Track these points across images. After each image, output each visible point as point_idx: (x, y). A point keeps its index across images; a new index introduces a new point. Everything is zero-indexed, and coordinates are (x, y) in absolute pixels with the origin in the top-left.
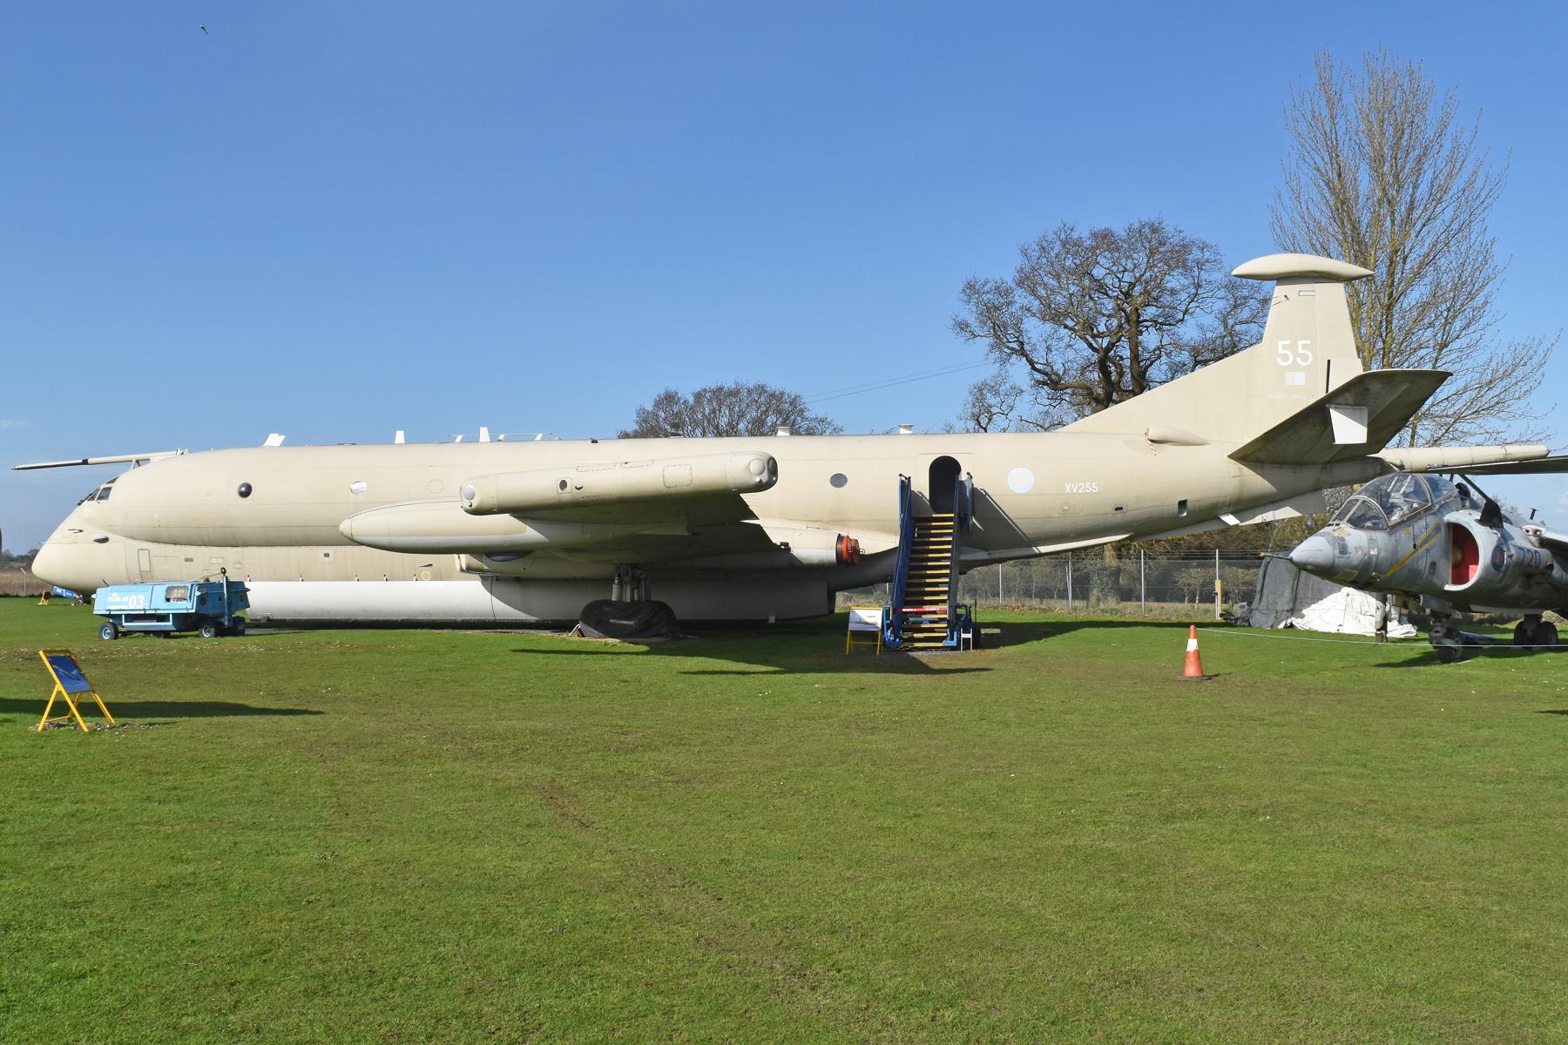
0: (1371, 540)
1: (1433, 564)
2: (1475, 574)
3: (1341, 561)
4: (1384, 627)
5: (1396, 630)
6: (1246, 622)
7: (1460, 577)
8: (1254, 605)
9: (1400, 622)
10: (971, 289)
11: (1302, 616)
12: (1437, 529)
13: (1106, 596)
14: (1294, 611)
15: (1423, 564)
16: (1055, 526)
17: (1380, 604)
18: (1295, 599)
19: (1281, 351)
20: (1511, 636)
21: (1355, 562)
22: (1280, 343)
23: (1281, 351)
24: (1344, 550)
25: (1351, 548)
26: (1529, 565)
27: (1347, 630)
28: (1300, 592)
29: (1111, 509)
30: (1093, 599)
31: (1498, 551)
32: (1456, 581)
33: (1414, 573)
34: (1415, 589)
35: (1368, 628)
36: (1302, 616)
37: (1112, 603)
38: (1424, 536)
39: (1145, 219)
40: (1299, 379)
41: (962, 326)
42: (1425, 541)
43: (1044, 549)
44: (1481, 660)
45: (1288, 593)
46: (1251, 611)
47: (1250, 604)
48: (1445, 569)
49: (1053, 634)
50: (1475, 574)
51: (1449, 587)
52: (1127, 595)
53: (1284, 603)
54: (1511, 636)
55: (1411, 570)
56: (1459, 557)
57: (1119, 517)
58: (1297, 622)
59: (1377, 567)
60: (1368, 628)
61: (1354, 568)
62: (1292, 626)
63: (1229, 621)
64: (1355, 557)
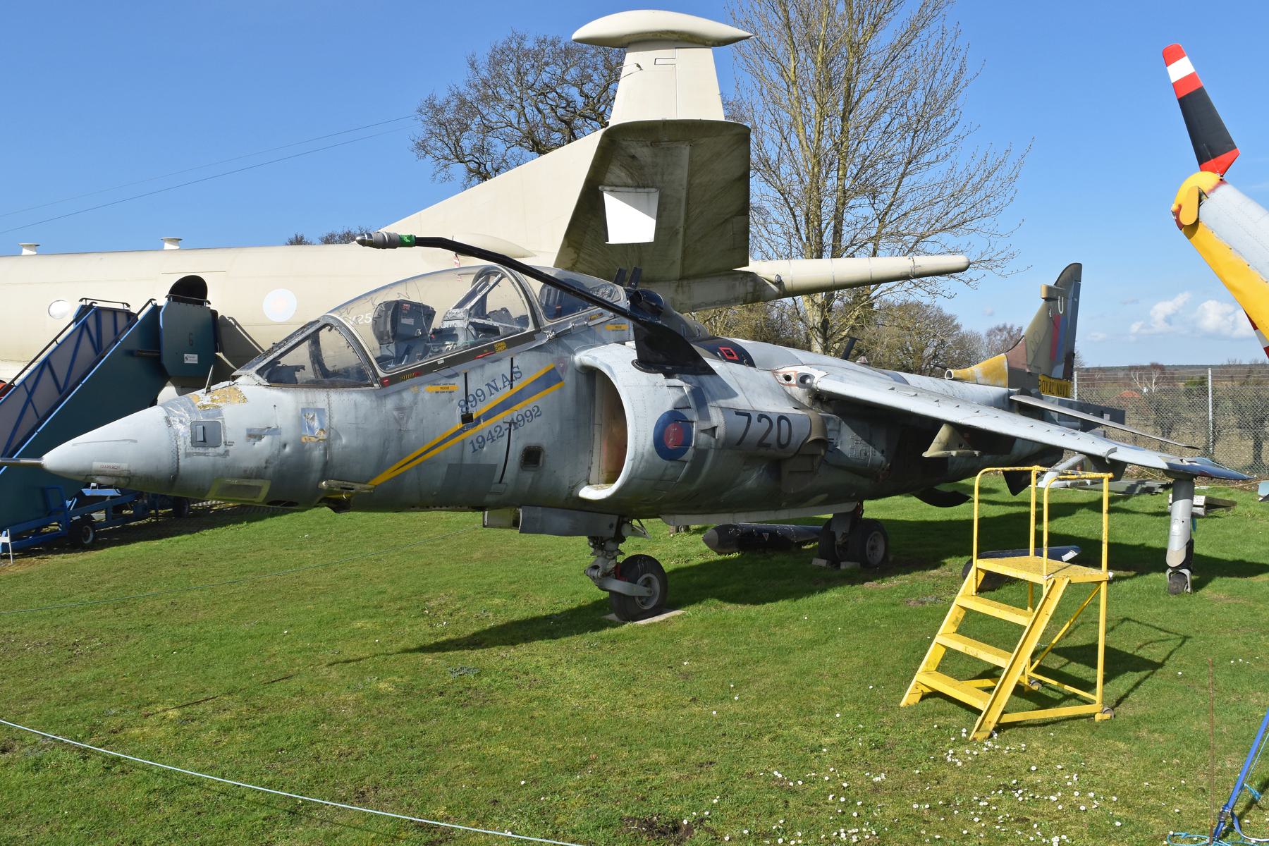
3: (205, 460)
12: (550, 378)
61: (258, 474)
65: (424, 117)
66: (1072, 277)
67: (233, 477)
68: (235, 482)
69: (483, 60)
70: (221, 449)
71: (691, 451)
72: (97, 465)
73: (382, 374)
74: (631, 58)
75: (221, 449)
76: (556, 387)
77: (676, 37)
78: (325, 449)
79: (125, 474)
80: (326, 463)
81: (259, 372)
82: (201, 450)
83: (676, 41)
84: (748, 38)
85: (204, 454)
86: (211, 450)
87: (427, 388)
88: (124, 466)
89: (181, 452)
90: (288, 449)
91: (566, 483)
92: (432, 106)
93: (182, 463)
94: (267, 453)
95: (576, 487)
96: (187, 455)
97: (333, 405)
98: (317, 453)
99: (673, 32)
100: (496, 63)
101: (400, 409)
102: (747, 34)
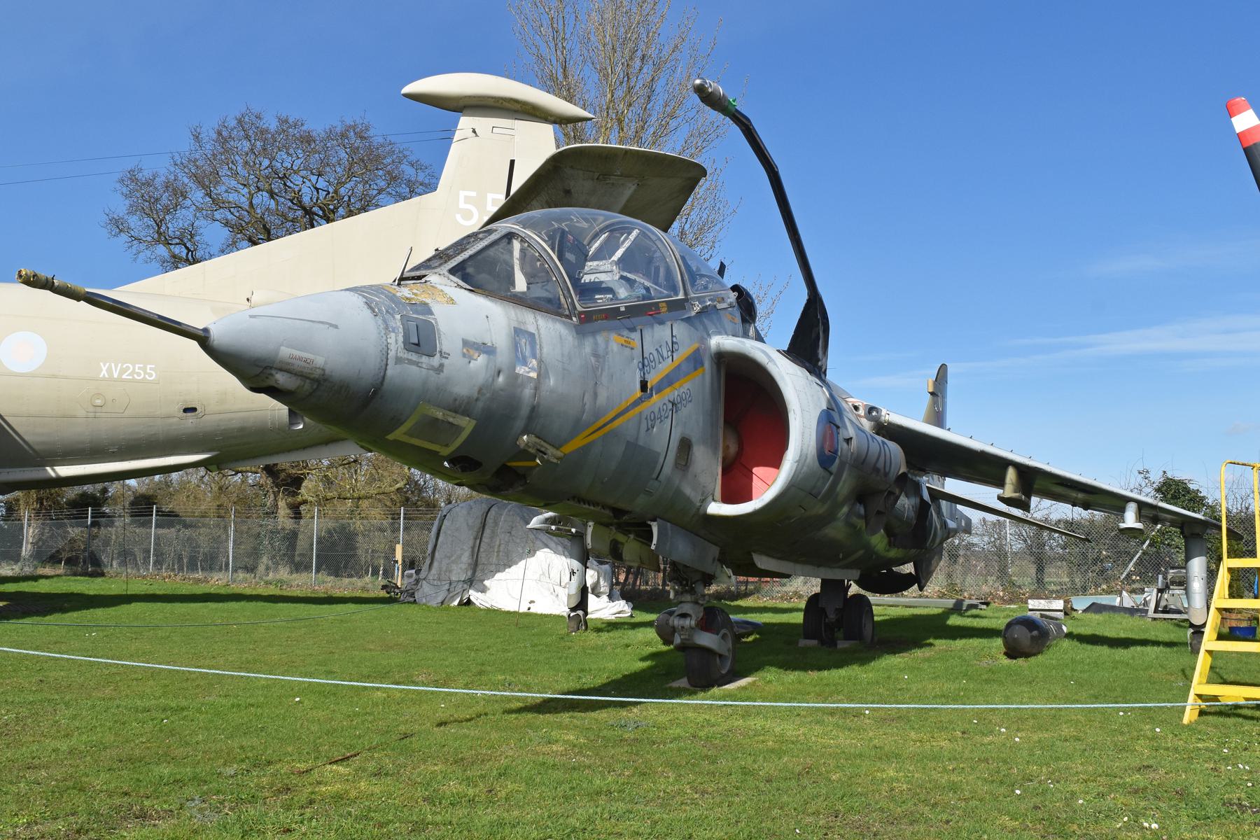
0: (518, 332)
1: (685, 446)
2: (768, 487)
3: (409, 373)
4: (582, 605)
5: (603, 608)
6: (410, 596)
7: (736, 490)
8: (422, 575)
9: (611, 597)
10: (136, 184)
11: (484, 590)
12: (695, 359)
13: (277, 564)
14: (474, 580)
15: (663, 439)
16: (79, 431)
17: (576, 564)
18: (475, 565)
19: (462, 205)
20: (798, 618)
21: (463, 389)
22: (463, 194)
23: (462, 205)
24: (422, 340)
25: (449, 340)
26: (876, 470)
27: (537, 609)
28: (482, 555)
29: (176, 409)
30: (261, 568)
31: (831, 419)
32: (728, 499)
33: (639, 460)
34: (640, 504)
35: (557, 604)
36: (484, 590)
37: (284, 573)
38: (665, 367)
39: (350, 122)
40: (467, 215)
41: (118, 225)
42: (668, 381)
43: (65, 471)
44: (771, 676)
45: (466, 558)
46: (417, 581)
47: (418, 572)
48: (708, 466)
49: (44, 613)
50: (768, 487)
51: (717, 508)
52: (300, 566)
53: (459, 572)
54: (798, 618)
55: (633, 448)
56: (733, 449)
57: (190, 422)
58: (474, 595)
59: (534, 418)
60: (557, 604)
61: (461, 407)
62: (469, 602)
63: (391, 597)
64: (466, 374)
65: (125, 190)
66: (943, 369)
67: (439, 406)
68: (439, 415)
69: (208, 134)
70: (436, 361)
71: (837, 461)
72: (285, 352)
73: (579, 308)
74: (466, 123)
75: (436, 361)
76: (700, 370)
77: (518, 107)
78: (536, 389)
79: (317, 374)
80: (534, 409)
81: (453, 271)
82: (414, 357)
83: (516, 111)
84: (590, 119)
85: (417, 364)
86: (424, 359)
87: (614, 336)
88: (319, 361)
89: (392, 354)
90: (501, 379)
91: (695, 497)
92: (133, 179)
93: (389, 372)
94: (481, 379)
95: (704, 502)
96: (399, 360)
97: (542, 331)
98: (528, 392)
99: (516, 101)
100: (222, 139)
101: (596, 355)
102: (591, 116)
